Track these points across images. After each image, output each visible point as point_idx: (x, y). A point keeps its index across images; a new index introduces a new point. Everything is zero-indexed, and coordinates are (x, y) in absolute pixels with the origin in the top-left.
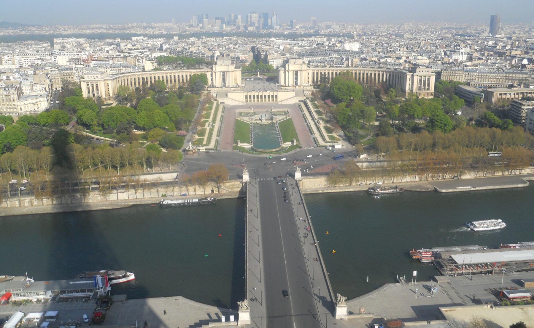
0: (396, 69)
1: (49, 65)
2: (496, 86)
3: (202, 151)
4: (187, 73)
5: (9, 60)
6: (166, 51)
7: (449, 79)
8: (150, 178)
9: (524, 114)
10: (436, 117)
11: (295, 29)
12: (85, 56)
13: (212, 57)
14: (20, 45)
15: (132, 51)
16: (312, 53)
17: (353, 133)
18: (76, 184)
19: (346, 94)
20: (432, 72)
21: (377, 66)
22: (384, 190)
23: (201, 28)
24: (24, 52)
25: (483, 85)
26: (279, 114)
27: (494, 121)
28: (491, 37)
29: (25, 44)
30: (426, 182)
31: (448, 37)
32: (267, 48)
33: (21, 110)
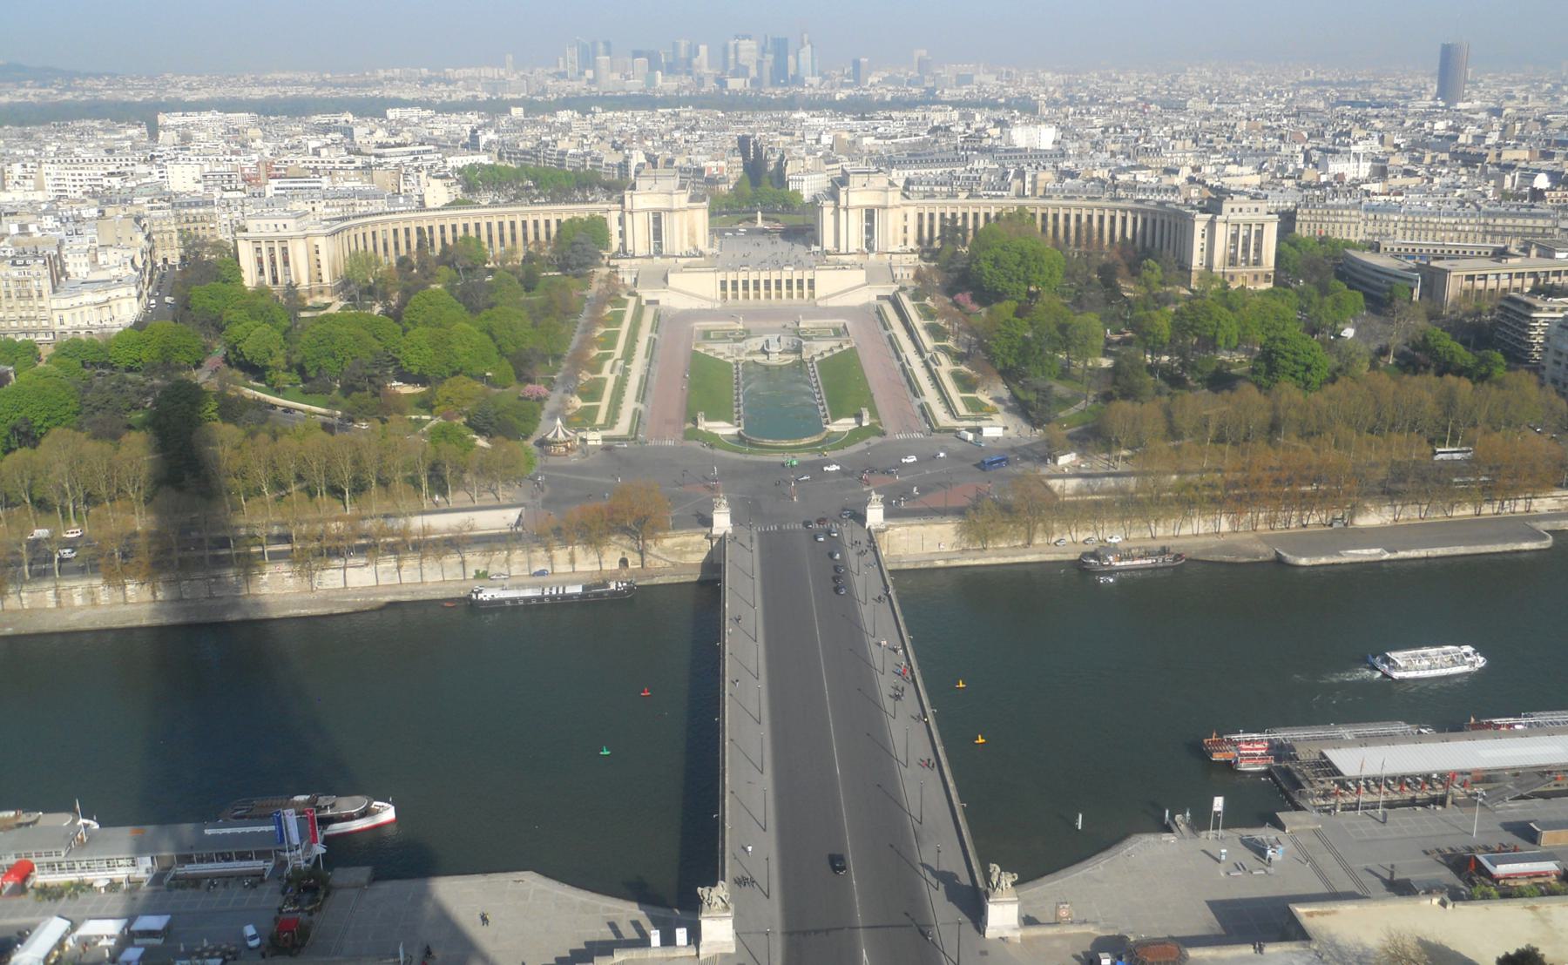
0: (1161, 204)
1: (145, 191)
2: (1457, 252)
3: (594, 443)
4: (549, 215)
5: (25, 178)
6: (487, 150)
7: (1317, 234)
8: (441, 523)
9: (1537, 336)
10: (1280, 345)
11: (867, 87)
12: (250, 165)
13: (624, 166)
14: (59, 132)
15: (387, 150)
16: (917, 156)
17: (1037, 390)
18: (224, 543)
19: (1015, 278)
20: (1269, 213)
21: (1107, 195)
22: (1128, 558)
23: (591, 82)
24: (69, 152)
25: (1417, 251)
26: (819, 335)
27: (1452, 357)
28: (1442, 108)
29: (73, 131)
30: (1251, 536)
31: (1314, 110)
32: (784, 142)
33: (62, 323)
